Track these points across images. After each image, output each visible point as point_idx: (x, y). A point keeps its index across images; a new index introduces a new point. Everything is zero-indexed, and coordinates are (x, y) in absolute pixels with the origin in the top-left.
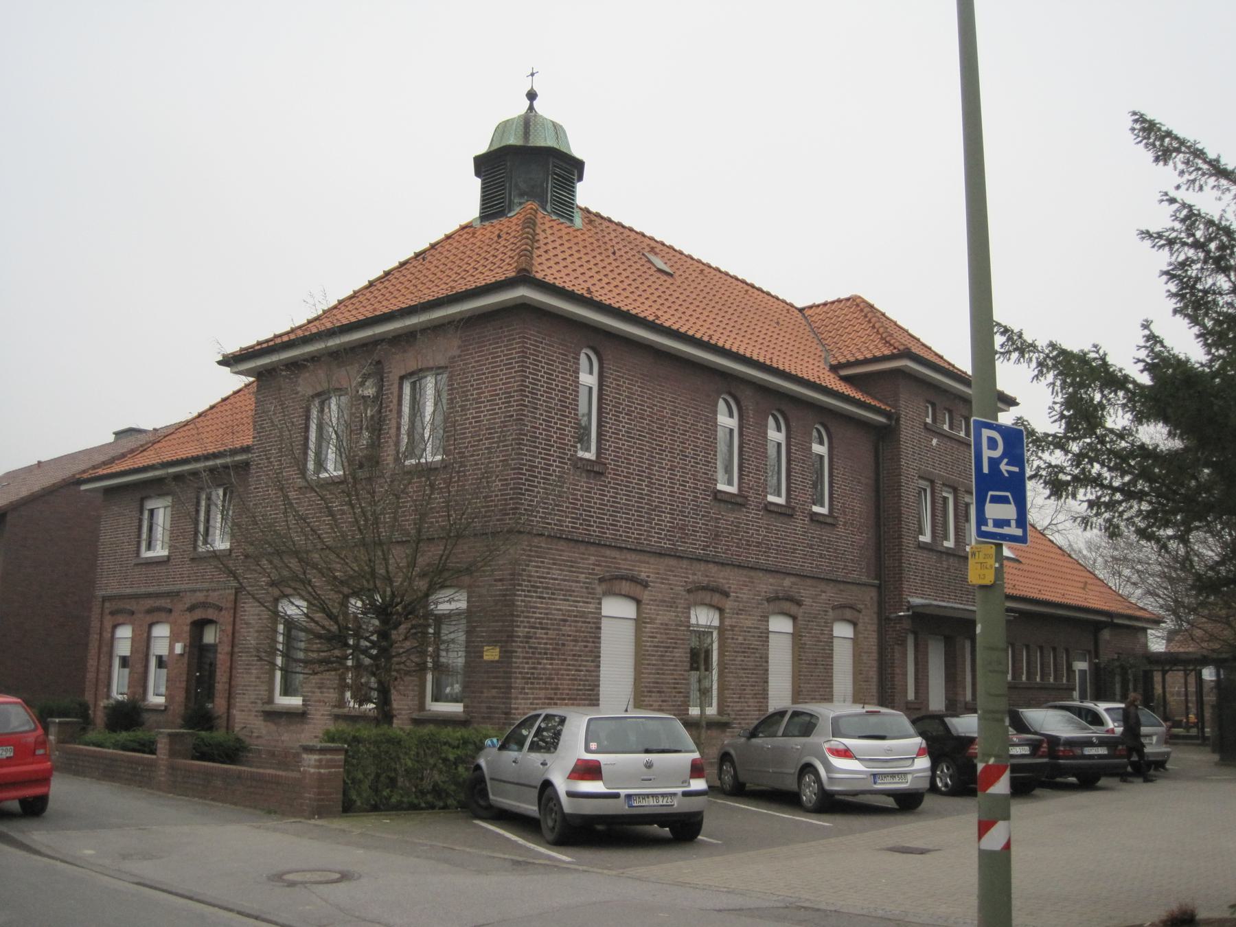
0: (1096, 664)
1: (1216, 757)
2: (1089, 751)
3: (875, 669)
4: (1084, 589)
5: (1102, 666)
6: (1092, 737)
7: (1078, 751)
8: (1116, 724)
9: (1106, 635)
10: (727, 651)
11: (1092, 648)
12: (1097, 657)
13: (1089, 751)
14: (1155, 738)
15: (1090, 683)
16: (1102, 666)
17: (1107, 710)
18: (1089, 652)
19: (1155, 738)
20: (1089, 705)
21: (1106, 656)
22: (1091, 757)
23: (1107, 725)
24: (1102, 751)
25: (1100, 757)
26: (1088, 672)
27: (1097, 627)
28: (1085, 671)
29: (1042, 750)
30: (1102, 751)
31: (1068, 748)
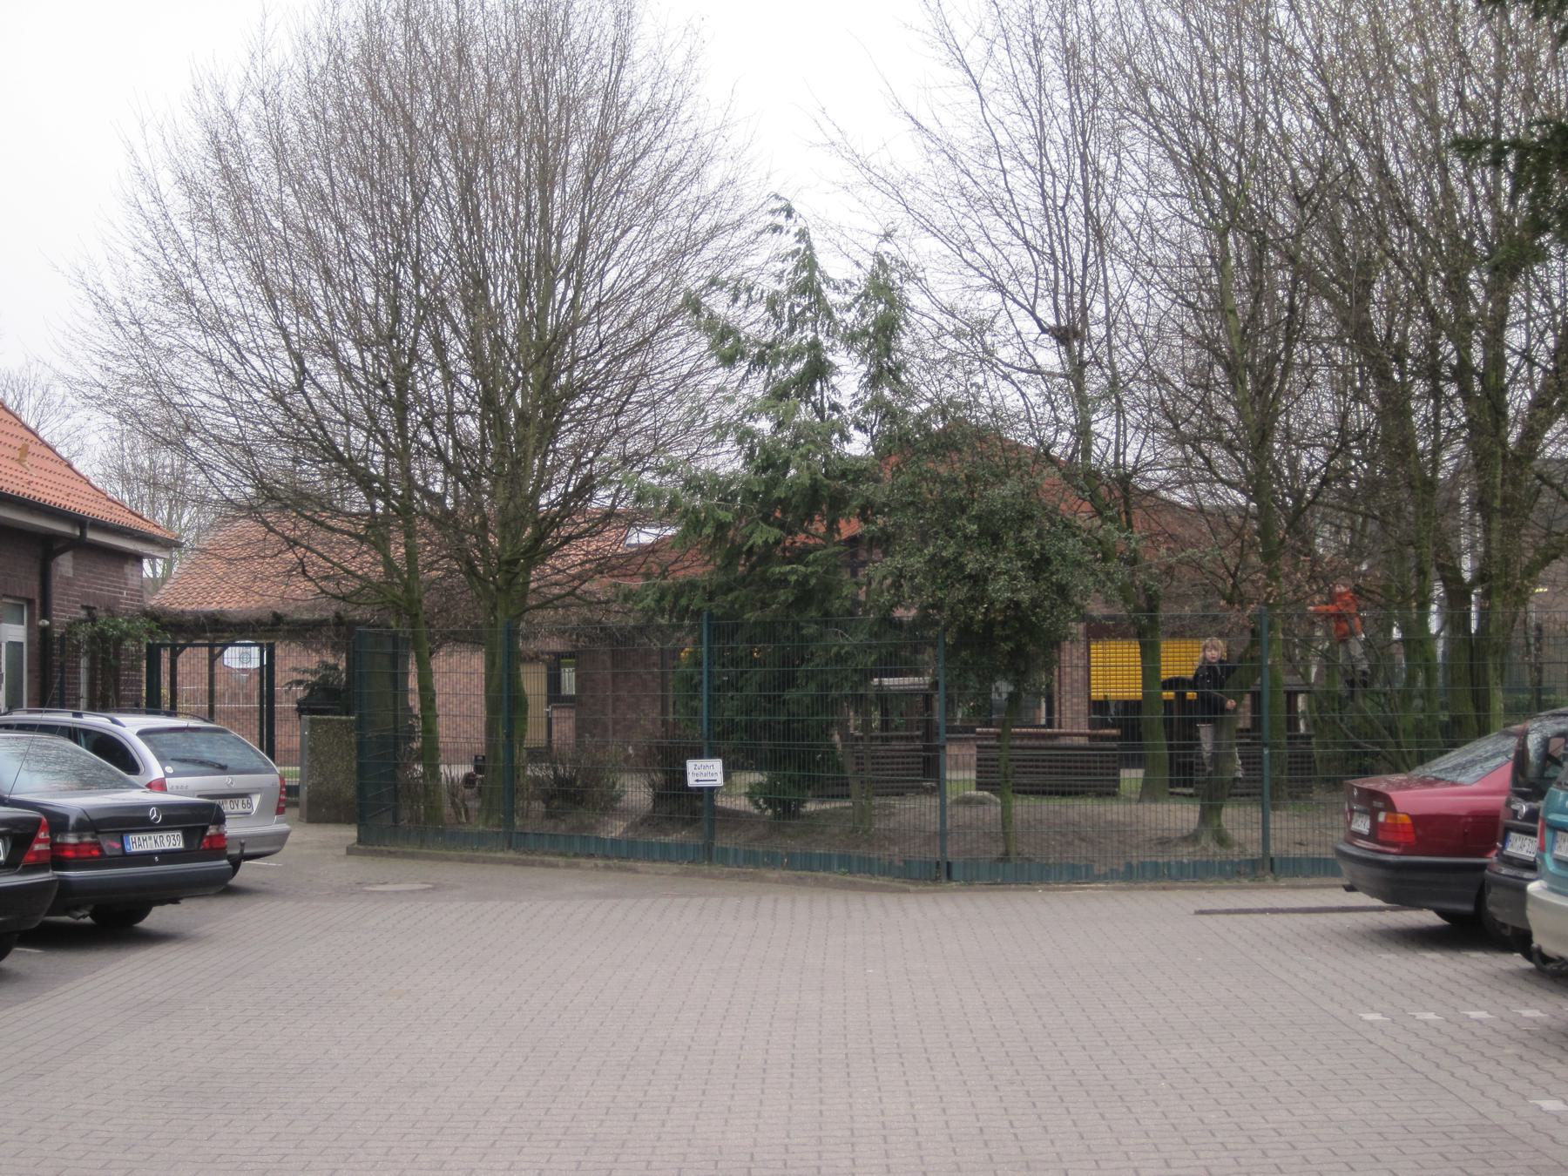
0: (45, 631)
1: (350, 833)
2: (139, 843)
3: (1172, 807)
4: (20, 461)
5: (57, 632)
6: (146, 807)
7: (110, 845)
8: (169, 769)
9: (65, 565)
10: (1389, 336)
11: (36, 596)
12: (45, 614)
13: (139, 843)
14: (256, 800)
15: (29, 671)
16: (57, 632)
17: (143, 734)
18: (30, 602)
19: (256, 800)
20: (97, 721)
21: (65, 611)
22: (146, 858)
23: (149, 772)
24: (172, 841)
25: (168, 856)
26: (1175, 705)
27: (45, 548)
28: (21, 644)
29: (37, 847)
30: (172, 841)
31: (87, 839)
